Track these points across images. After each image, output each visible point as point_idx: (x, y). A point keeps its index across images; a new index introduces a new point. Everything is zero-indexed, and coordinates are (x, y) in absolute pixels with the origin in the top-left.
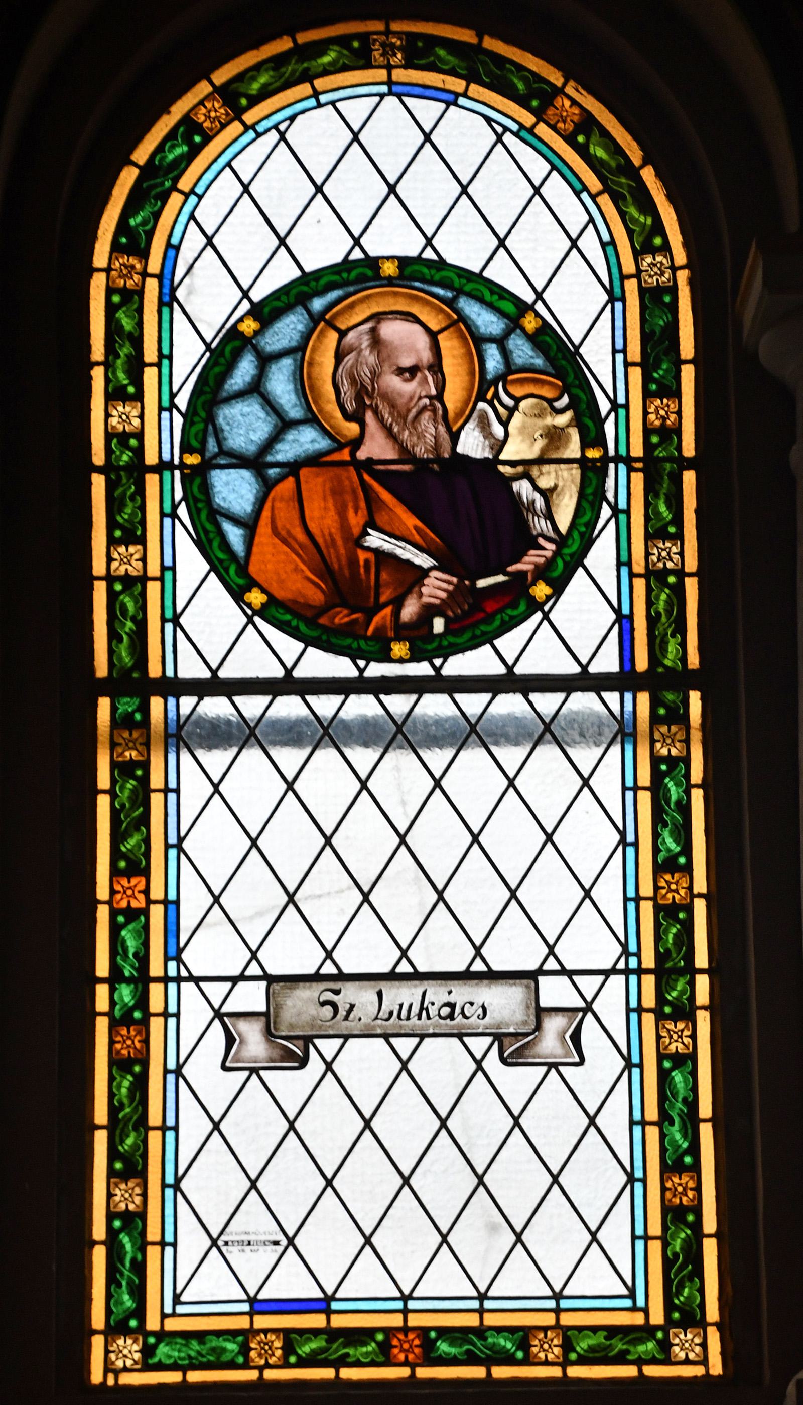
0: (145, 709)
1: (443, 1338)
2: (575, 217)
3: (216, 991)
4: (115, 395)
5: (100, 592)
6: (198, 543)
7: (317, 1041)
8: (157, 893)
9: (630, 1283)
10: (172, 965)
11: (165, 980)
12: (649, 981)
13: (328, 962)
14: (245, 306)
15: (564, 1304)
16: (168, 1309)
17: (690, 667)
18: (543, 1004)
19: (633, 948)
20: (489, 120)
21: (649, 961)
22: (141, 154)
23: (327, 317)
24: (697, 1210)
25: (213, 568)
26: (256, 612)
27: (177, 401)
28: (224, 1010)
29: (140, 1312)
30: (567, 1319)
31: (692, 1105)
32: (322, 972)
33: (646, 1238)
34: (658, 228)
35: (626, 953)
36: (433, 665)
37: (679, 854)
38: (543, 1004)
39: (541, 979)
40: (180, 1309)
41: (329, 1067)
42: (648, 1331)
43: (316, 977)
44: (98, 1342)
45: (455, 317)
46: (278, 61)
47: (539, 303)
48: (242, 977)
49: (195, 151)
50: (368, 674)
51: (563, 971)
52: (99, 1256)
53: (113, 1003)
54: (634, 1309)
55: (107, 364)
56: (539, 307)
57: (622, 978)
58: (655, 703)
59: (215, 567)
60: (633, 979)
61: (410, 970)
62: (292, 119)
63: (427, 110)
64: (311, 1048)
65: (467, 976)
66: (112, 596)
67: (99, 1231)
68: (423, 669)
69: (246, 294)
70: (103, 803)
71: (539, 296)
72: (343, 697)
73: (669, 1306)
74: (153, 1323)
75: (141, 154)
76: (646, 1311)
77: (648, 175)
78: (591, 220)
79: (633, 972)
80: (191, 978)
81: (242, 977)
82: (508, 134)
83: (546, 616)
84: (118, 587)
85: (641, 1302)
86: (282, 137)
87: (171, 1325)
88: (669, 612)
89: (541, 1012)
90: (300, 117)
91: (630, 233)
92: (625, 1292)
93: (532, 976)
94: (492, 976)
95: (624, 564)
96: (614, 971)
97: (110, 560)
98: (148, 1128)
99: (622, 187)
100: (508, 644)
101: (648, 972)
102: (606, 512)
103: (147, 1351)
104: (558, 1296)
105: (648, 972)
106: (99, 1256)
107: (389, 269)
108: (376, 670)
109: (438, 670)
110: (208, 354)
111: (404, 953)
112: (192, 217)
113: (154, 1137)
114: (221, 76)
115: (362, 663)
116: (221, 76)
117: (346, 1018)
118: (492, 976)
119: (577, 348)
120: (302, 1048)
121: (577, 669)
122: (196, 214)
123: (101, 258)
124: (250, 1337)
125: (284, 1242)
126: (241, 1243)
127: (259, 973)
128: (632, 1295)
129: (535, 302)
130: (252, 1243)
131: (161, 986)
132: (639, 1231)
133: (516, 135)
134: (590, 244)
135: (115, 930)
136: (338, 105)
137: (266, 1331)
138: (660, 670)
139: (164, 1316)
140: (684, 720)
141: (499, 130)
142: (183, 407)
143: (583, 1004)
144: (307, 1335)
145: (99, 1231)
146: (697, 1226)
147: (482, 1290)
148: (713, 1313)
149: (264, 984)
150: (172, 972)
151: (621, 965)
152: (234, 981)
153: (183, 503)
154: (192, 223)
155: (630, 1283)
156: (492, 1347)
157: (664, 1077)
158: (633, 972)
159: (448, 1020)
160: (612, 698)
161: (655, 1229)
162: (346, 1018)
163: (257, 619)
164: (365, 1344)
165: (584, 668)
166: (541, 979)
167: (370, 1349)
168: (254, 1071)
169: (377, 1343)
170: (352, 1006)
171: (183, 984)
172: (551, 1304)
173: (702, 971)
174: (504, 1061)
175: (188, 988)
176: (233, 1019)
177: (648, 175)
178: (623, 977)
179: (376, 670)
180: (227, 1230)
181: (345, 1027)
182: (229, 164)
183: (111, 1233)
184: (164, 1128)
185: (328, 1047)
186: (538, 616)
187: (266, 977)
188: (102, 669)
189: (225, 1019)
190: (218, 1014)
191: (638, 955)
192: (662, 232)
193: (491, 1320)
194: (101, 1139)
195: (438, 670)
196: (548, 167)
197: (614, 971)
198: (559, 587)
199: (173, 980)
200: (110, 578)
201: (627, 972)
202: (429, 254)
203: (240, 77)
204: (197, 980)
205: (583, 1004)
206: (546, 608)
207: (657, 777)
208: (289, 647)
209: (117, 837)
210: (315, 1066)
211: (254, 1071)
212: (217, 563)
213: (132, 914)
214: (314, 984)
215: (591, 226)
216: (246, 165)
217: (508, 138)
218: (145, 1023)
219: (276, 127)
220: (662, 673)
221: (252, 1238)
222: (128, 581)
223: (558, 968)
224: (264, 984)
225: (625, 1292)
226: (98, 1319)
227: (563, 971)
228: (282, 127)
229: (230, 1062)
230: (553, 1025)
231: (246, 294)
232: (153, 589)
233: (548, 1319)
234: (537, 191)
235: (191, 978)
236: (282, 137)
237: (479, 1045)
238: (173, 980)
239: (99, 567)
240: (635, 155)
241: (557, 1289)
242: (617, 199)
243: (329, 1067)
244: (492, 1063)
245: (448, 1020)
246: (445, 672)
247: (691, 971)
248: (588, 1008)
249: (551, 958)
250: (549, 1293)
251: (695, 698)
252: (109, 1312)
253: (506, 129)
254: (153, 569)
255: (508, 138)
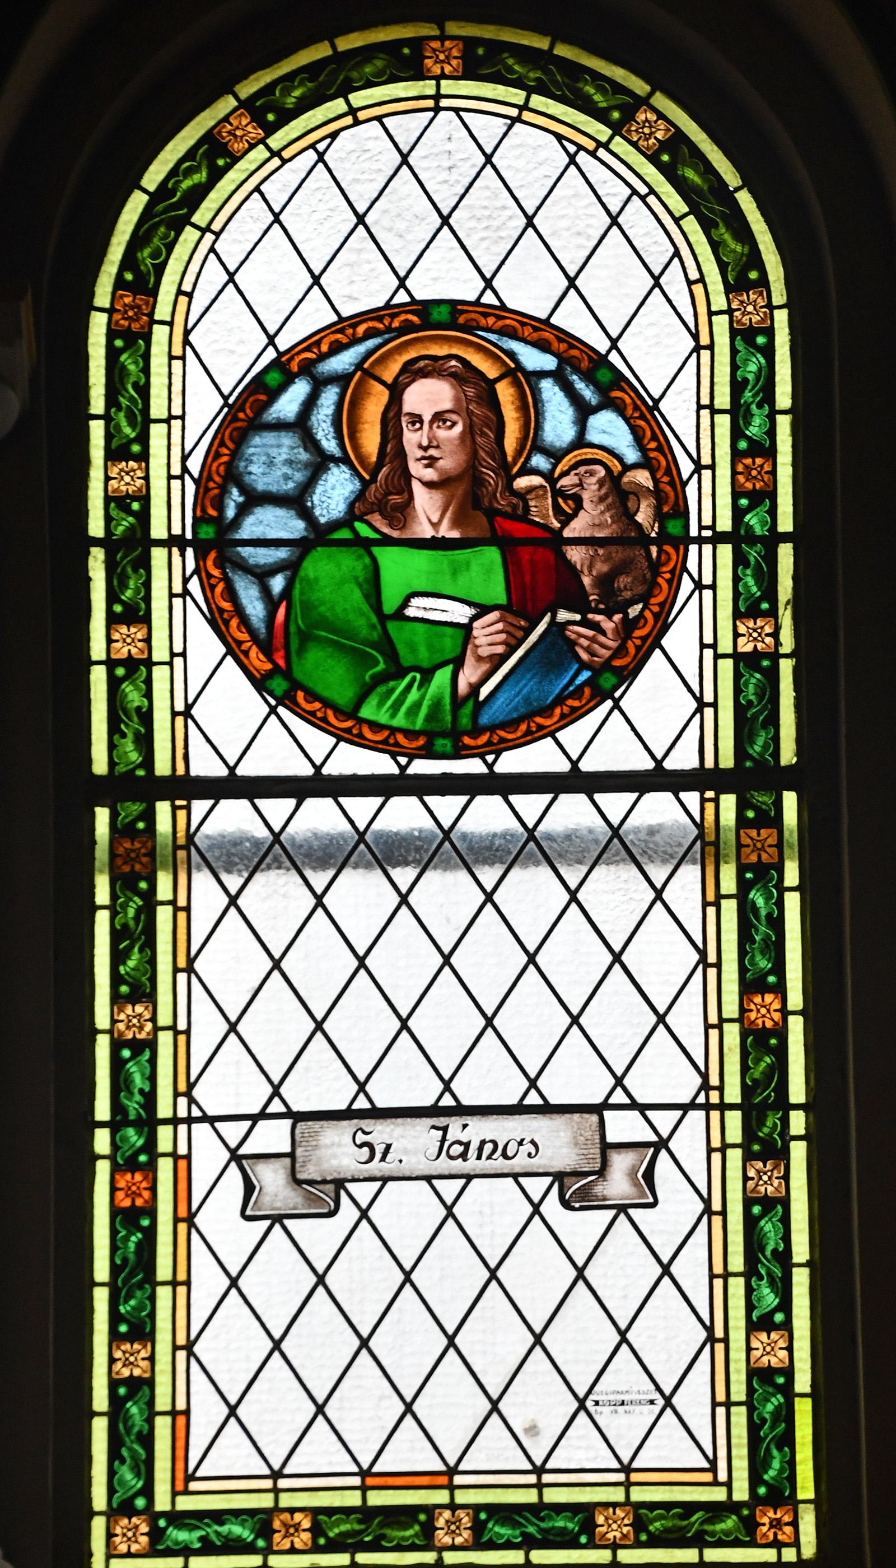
0: (149, 817)
1: (497, 1517)
2: (658, 252)
3: (233, 1132)
4: (115, 453)
5: (98, 676)
6: (212, 623)
7: (348, 1185)
8: (164, 1018)
9: (710, 1455)
10: (182, 1102)
11: (175, 1121)
12: (734, 1120)
13: (533, 1091)
14: (271, 354)
15: (547, 1478)
16: (180, 1486)
17: (722, 766)
18: (610, 1139)
19: (714, 1081)
20: (560, 137)
21: (733, 1094)
22: (153, 177)
23: (366, 366)
24: (789, 1372)
25: (230, 652)
26: (280, 702)
27: (189, 464)
28: (242, 1151)
29: (148, 1491)
30: (638, 1495)
31: (784, 1257)
32: (526, 1102)
33: (728, 1404)
34: (755, 259)
35: (705, 1086)
36: (485, 762)
37: (770, 972)
38: (610, 1139)
39: (607, 1114)
40: (193, 1486)
41: (364, 1214)
42: (730, 1507)
43: (348, 1114)
44: (98, 1525)
45: (513, 365)
46: (312, 70)
47: (614, 352)
48: (264, 1115)
49: (216, 175)
50: (410, 771)
51: (634, 1105)
52: (100, 1428)
53: (114, 1146)
54: (715, 1483)
55: (107, 417)
56: (614, 358)
57: (702, 1114)
58: (741, 807)
59: (233, 650)
60: (715, 1115)
61: (539, 1101)
62: (334, 136)
63: (488, 129)
64: (343, 1193)
65: (519, 1109)
66: (114, 684)
67: (100, 1400)
68: (474, 766)
69: (271, 340)
70: (102, 921)
71: (614, 343)
72: (211, 802)
73: (755, 1478)
74: (162, 1503)
75: (153, 177)
76: (729, 1484)
77: (745, 200)
78: (677, 254)
79: (715, 1107)
80: (205, 1118)
81: (264, 1115)
82: (582, 153)
83: (616, 706)
84: (120, 672)
85: (722, 1476)
86: (321, 157)
87: (185, 1503)
88: (761, 697)
89: (606, 1148)
90: (342, 134)
91: (722, 267)
92: (706, 1465)
93: (598, 1109)
94: (547, 1109)
95: (708, 646)
96: (692, 1105)
97: (110, 641)
98: (155, 1284)
99: (716, 215)
100: (574, 736)
101: (732, 1107)
102: (687, 585)
103: (156, 1535)
104: (627, 1469)
105: (732, 1107)
106: (100, 1428)
107: (441, 314)
108: (421, 767)
109: (490, 766)
110: (226, 410)
111: (533, 1083)
112: (212, 250)
113: (163, 1294)
114: (247, 89)
115: (403, 760)
116: (247, 89)
117: (383, 1159)
118: (547, 1109)
119: (657, 402)
120: (332, 1195)
121: (651, 765)
122: (216, 246)
123: (103, 296)
124: (143, 1517)
125: (661, 1402)
126: (610, 1403)
127: (283, 1109)
128: (713, 1468)
129: (609, 352)
130: (626, 1403)
131: (170, 1128)
132: (721, 1397)
133: (593, 154)
134: (674, 282)
135: (117, 1065)
136: (385, 120)
137: (292, 1511)
138: (748, 764)
139: (174, 1494)
140: (777, 821)
141: (572, 149)
142: (195, 471)
143: (654, 1138)
144: (244, 1517)
145: (100, 1400)
146: (788, 1391)
147: (276, 1467)
148: (806, 1488)
149: (288, 1123)
150: (182, 1113)
151: (701, 1099)
152: (253, 1119)
153: (195, 578)
154: (212, 256)
155: (710, 1455)
156: (515, 1525)
157: (750, 1223)
158: (715, 1107)
159: (460, 1160)
160: (691, 799)
161: (739, 1392)
162: (383, 1159)
163: (281, 710)
164: (406, 1527)
165: (659, 763)
166: (607, 1114)
167: (336, 1531)
168: (278, 1219)
169: (421, 1524)
170: (389, 1147)
171: (194, 1126)
172: (532, 1479)
173: (797, 1107)
174: (566, 1204)
175: (201, 1130)
176: (249, 1161)
177: (745, 200)
178: (703, 1113)
179: (421, 767)
180: (596, 1389)
181: (376, 1167)
182: (257, 189)
183: (116, 1403)
184: (174, 1283)
185: (363, 1192)
186: (609, 704)
187: (289, 1114)
188: (100, 766)
189: (244, 1162)
190: (235, 1156)
191: (721, 1089)
192: (759, 264)
193: (552, 1496)
194: (101, 1298)
195: (490, 766)
196: (629, 191)
197: (692, 1105)
198: (629, 674)
199: (183, 1121)
200: (110, 664)
201: (707, 1107)
202: (489, 298)
203: (268, 90)
204: (212, 1120)
205: (654, 1138)
206: (617, 694)
207: (744, 887)
208: (318, 742)
209: (117, 957)
210: (348, 1213)
211: (278, 1219)
212: (234, 645)
213: (138, 1047)
214: (345, 1123)
215: (676, 260)
216: (276, 190)
217: (582, 158)
218: (151, 1169)
219: (313, 146)
220: (750, 768)
221: (626, 1398)
222: (131, 664)
223: (283, 1110)
224: (288, 1123)
225: (706, 1465)
226: (99, 1499)
227: (634, 1105)
228: (321, 147)
229: (648, 1198)
230: (621, 1163)
231: (271, 340)
232: (160, 674)
233: (618, 1495)
234: (614, 221)
235: (205, 1118)
236: (321, 157)
237: (536, 1186)
238: (183, 1121)
239: (98, 649)
240: (731, 177)
241: (626, 1461)
242: (707, 225)
243: (364, 1214)
244: (552, 1207)
245: (460, 1160)
246: (498, 768)
247: (785, 1106)
248: (662, 1144)
249: (276, 1100)
250: (267, 1472)
251: (790, 800)
252: (111, 1491)
253: (580, 148)
254: (160, 653)
255: (582, 158)
